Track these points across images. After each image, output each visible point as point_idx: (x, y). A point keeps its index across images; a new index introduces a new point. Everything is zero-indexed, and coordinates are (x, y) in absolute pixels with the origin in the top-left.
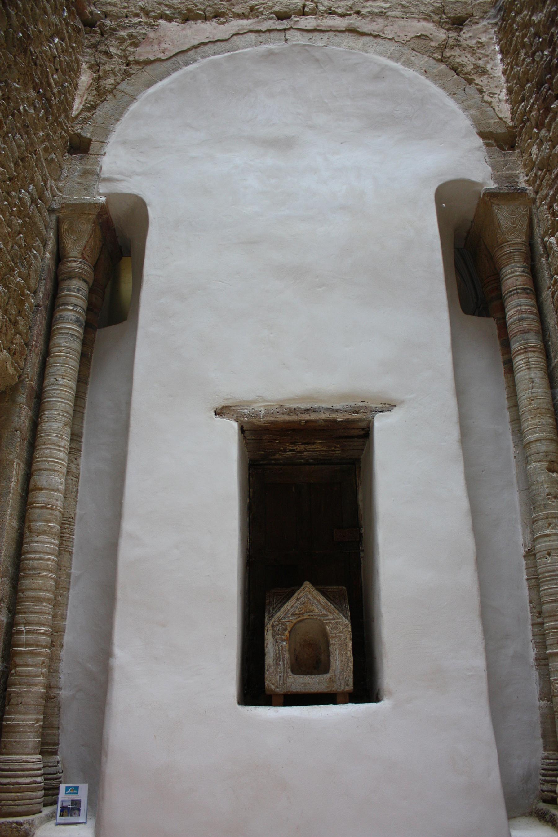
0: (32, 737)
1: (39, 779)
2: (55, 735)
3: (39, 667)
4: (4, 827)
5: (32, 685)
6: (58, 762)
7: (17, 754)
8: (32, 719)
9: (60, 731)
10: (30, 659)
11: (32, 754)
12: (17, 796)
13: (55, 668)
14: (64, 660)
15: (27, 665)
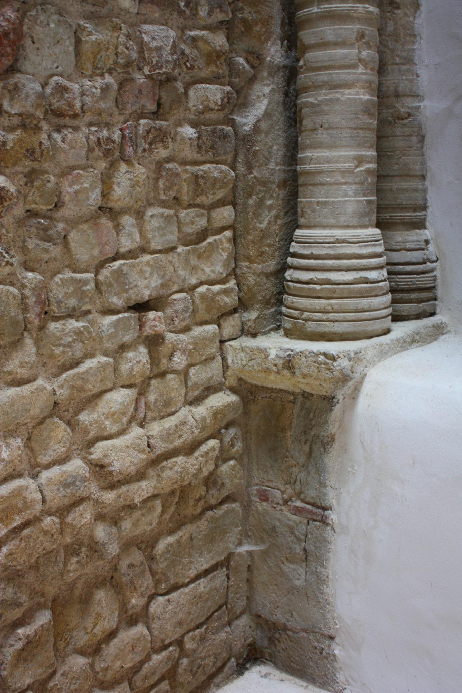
0: (351, 193)
1: (373, 275)
2: (416, 190)
3: (352, 45)
4: (304, 359)
5: (340, 86)
6: (427, 242)
7: (324, 227)
8: (347, 157)
9: (426, 183)
10: (329, 31)
11: (355, 227)
12: (331, 305)
13: (404, 54)
14: (424, 36)
15: (324, 45)
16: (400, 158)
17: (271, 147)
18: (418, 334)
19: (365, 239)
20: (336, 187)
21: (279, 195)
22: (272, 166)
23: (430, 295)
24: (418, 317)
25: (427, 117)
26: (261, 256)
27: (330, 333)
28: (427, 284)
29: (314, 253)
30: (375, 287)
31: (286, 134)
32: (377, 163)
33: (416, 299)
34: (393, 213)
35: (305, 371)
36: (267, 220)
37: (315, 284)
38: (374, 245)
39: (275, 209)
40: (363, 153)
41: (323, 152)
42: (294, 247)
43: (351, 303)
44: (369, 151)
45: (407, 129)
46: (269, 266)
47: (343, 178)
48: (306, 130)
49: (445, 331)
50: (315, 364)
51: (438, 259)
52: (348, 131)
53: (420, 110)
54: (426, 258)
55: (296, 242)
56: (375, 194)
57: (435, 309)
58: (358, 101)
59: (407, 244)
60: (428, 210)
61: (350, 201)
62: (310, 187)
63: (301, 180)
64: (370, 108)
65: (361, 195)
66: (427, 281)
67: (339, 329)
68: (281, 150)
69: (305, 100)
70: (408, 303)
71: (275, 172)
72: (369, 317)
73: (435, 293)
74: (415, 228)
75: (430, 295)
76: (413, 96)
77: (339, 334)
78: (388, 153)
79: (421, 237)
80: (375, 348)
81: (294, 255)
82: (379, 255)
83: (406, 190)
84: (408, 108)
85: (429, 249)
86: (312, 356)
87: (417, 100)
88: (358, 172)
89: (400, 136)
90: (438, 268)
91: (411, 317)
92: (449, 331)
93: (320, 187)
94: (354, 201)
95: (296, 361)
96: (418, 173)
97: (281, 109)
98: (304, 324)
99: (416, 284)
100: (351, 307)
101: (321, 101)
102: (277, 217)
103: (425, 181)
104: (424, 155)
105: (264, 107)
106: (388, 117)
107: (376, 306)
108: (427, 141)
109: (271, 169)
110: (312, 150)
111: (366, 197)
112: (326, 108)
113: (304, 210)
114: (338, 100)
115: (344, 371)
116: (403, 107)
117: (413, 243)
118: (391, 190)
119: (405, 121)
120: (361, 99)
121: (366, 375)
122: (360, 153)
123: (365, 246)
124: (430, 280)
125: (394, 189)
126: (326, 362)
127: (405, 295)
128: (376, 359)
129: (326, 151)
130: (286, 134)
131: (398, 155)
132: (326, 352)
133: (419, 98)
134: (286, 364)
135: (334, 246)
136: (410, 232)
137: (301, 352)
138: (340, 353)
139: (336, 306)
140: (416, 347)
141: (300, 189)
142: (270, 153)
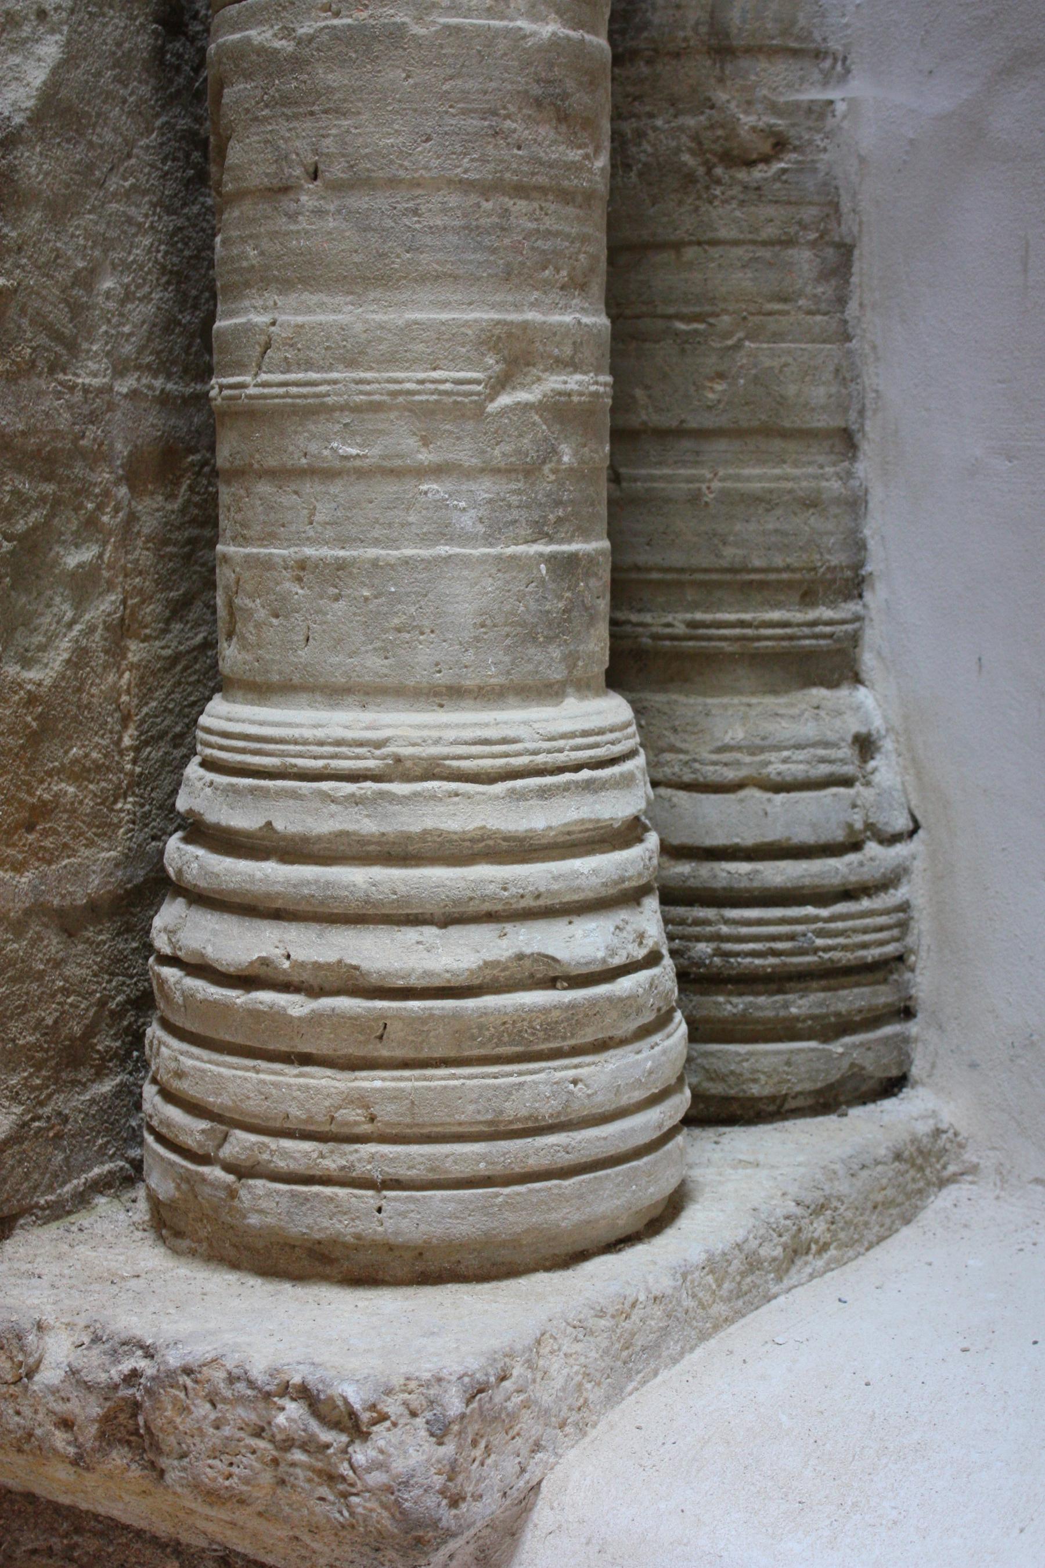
0: (467, 521)
1: (583, 941)
2: (812, 503)
4: (203, 1409)
6: (865, 745)
7: (335, 692)
8: (443, 334)
9: (862, 468)
11: (489, 695)
12: (361, 1100)
16: (738, 346)
17: (86, 279)
18: (820, 1209)
19: (541, 759)
20: (390, 488)
21: (132, 518)
22: (90, 373)
23: (882, 996)
24: (827, 1101)
25: (862, 160)
26: (30, 828)
27: (360, 1245)
28: (865, 946)
29: (279, 826)
30: (593, 1002)
31: (170, 222)
32: (613, 371)
33: (814, 1018)
34: (707, 610)
35: (211, 1471)
36: (65, 644)
37: (286, 987)
38: (588, 786)
39: (110, 586)
40: (531, 315)
41: (321, 305)
42: (199, 792)
43: (469, 1089)
44: (566, 308)
45: (770, 211)
46: (77, 874)
47: (426, 442)
48: (241, 195)
49: (952, 1169)
50: (261, 1444)
51: (916, 828)
52: (454, 200)
53: (830, 122)
54: (859, 826)
55: (208, 764)
56: (603, 527)
57: (905, 1060)
58: (502, 45)
59: (773, 756)
60: (868, 596)
61: (466, 562)
62: (264, 488)
63: (228, 450)
64: (570, 85)
65: (524, 531)
66: (865, 931)
67: (404, 1224)
68: (146, 298)
69: (237, 36)
70: (780, 1040)
71: (111, 407)
72: (565, 1159)
73: (902, 987)
74: (809, 681)
75: (882, 996)
76: (795, 53)
77: (405, 1247)
78: (681, 326)
79: (838, 723)
80: (590, 1332)
81: (199, 832)
82: (630, 833)
83: (762, 502)
84: (774, 109)
85: (876, 778)
86: (240, 1400)
87: (816, 76)
88: (504, 411)
89: (736, 243)
90: (918, 865)
91: (791, 1104)
92: (973, 1169)
93: (309, 487)
94: (483, 560)
95: (163, 1416)
96: (822, 421)
97: (145, 90)
98: (233, 1194)
99: (816, 951)
100: (468, 1114)
101: (311, 39)
102: (121, 629)
103: (854, 459)
104: (848, 338)
105: (37, 76)
106: (678, 151)
107: (599, 1098)
108: (865, 266)
109: (86, 390)
110: (272, 297)
111: (551, 539)
112: (335, 78)
113: (237, 601)
114: (396, 34)
115: (409, 1498)
116: (749, 103)
117: (801, 755)
118: (694, 499)
119: (759, 173)
120: (520, 36)
121: (535, 1489)
122: (514, 317)
123: (544, 793)
124: (881, 929)
125: (709, 497)
126: (312, 1438)
127: (762, 1000)
128: (594, 1394)
129: (339, 299)
130: (170, 222)
131: (727, 335)
132: (312, 1381)
133: (827, 64)
134: (122, 1417)
135: (382, 795)
136: (783, 700)
137: (188, 1371)
138: (389, 1392)
139: (391, 1108)
140: (812, 1277)
141: (225, 494)
142: (76, 309)
